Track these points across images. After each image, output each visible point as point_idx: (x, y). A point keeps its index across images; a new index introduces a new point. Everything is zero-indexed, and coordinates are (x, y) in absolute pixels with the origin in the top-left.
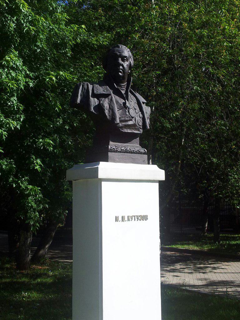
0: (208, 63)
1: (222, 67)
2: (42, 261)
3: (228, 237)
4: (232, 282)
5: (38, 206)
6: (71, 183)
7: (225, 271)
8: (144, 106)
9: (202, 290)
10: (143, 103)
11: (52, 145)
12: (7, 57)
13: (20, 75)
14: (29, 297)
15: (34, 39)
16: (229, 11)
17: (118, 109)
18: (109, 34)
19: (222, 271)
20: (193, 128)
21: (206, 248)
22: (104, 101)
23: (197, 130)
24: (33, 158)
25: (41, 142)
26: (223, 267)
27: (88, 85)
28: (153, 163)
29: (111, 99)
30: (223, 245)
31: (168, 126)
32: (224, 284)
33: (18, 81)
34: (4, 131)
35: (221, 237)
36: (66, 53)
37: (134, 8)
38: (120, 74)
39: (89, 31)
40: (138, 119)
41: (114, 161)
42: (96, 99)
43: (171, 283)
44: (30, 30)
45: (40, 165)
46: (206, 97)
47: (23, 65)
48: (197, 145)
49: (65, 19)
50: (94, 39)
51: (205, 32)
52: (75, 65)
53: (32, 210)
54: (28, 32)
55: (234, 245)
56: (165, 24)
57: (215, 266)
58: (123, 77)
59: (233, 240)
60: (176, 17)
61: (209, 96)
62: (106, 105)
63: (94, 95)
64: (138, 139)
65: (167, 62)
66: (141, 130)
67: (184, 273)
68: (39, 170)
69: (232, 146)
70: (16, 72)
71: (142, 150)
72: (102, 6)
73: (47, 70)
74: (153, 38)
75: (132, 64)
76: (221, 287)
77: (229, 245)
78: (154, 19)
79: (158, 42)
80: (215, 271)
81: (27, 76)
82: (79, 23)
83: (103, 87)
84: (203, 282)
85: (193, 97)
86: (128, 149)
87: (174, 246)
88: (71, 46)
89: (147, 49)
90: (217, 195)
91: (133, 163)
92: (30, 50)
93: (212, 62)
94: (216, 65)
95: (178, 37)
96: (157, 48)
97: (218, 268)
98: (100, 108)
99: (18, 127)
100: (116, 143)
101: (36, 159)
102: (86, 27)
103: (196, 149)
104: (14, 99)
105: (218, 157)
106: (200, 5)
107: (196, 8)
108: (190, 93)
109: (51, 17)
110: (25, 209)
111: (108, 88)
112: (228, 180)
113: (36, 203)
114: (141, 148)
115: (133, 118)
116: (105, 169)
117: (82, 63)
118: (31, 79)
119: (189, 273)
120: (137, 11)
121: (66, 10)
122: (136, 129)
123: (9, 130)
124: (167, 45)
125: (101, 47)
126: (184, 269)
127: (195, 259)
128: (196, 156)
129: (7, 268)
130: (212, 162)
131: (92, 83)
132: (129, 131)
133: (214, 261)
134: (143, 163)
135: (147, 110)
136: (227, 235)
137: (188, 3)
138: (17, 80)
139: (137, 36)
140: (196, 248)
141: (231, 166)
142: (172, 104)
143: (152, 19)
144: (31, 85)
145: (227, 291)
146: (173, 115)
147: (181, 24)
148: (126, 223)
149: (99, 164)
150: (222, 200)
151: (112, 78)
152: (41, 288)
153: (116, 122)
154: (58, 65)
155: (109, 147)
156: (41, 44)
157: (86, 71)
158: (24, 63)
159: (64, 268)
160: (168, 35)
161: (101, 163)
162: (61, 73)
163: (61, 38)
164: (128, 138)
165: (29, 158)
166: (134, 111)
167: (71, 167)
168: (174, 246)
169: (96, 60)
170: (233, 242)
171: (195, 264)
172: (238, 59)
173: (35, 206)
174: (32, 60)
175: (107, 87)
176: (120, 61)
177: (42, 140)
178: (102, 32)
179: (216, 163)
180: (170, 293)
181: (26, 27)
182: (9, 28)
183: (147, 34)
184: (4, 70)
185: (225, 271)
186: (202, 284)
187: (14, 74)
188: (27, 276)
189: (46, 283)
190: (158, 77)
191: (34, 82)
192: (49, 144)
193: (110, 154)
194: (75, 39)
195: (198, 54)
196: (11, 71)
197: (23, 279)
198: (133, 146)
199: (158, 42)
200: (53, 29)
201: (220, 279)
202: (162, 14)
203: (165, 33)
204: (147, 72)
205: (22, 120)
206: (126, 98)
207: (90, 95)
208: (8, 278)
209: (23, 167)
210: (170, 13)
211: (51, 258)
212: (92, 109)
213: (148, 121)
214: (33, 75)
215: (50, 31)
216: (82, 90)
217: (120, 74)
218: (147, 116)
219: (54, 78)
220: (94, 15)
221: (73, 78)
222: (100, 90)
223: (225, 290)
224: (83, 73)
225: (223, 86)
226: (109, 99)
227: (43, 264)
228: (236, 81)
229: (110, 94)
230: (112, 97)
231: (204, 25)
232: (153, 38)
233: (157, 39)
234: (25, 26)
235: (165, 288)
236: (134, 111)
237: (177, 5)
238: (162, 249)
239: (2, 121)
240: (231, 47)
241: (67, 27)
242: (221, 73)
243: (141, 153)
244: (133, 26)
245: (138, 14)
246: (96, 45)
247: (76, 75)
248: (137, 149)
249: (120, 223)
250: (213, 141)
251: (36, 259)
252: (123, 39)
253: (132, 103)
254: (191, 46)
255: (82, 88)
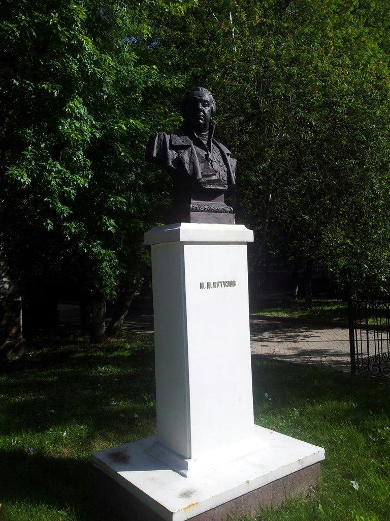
0: (298, 106)
1: (314, 110)
2: (117, 334)
3: (321, 302)
4: (326, 351)
5: (114, 272)
6: (148, 247)
7: (319, 339)
8: (228, 158)
9: (293, 360)
10: (228, 154)
11: (126, 203)
12: (70, 103)
13: (86, 126)
14: (106, 372)
15: (100, 83)
16: (321, 44)
17: (200, 162)
18: (184, 74)
19: (315, 339)
20: (282, 182)
21: (296, 315)
22: (183, 154)
23: (286, 184)
24: (105, 219)
25: (112, 201)
26: (316, 335)
27: (164, 135)
28: (238, 222)
29: (192, 151)
30: (315, 311)
31: (254, 178)
32: (318, 353)
33: (83, 132)
34: (72, 189)
35: (313, 302)
36: (136, 99)
37: (212, 44)
38: (201, 121)
39: (161, 72)
40: (222, 173)
41: (197, 221)
42: (174, 152)
43: (260, 353)
44: (95, 73)
45: (114, 226)
46: (296, 145)
47: (88, 114)
48: (287, 201)
49: (133, 59)
50: (167, 82)
51: (295, 70)
52: (146, 112)
53: (107, 276)
54: (94, 73)
55: (328, 311)
56: (248, 62)
57: (307, 334)
58: (205, 125)
59: (327, 305)
60: (261, 53)
61: (300, 144)
62: (186, 158)
63: (172, 147)
64: (223, 195)
65: (252, 106)
66: (226, 186)
67: (274, 342)
68: (113, 231)
69: (325, 201)
70: (81, 123)
71: (228, 209)
72: (175, 42)
73: (114, 118)
74: (234, 79)
75: (214, 110)
76: (314, 356)
77: (322, 310)
78: (236, 55)
79: (241, 83)
80: (307, 339)
81: (93, 126)
82: (149, 63)
83: (182, 137)
84: (295, 351)
85: (282, 145)
86: (212, 207)
87: (261, 314)
88: (142, 90)
89: (228, 92)
90: (309, 256)
91: (217, 223)
92: (95, 96)
93: (302, 105)
94: (309, 109)
95: (263, 77)
96: (240, 90)
97: (311, 336)
98: (179, 161)
99: (87, 185)
100: (198, 201)
101: (109, 220)
102: (158, 67)
103: (285, 205)
104: (80, 153)
105: (311, 214)
106: (288, 38)
107: (284, 41)
108: (279, 142)
109: (118, 57)
110: (98, 277)
111: (188, 138)
112: (321, 240)
113: (111, 269)
114: (226, 206)
115: (216, 172)
116: (187, 230)
117: (155, 109)
118: (97, 129)
119: (279, 342)
120: (215, 47)
121: (134, 48)
122: (221, 185)
123: (78, 188)
124: (251, 86)
125: (176, 90)
126: (273, 337)
127: (285, 327)
128: (285, 214)
129: (81, 342)
130: (304, 220)
131: (169, 133)
132: (213, 187)
133: (306, 329)
134: (230, 222)
135: (232, 162)
136: (333, 300)
137: (274, 36)
138: (82, 132)
139: (217, 78)
140: (286, 315)
141: (325, 224)
142: (257, 155)
143: (233, 56)
144: (98, 135)
145: (321, 361)
146: (259, 167)
147: (267, 61)
148: (212, 290)
149: (180, 226)
150: (314, 262)
151: (192, 126)
152: (119, 362)
153: (198, 178)
154: (127, 113)
155: (191, 206)
156: (108, 89)
157: (159, 119)
158: (90, 112)
159: (142, 340)
160: (252, 74)
161: (182, 224)
162: (131, 121)
163: (130, 82)
164: (211, 195)
165: (101, 219)
166: (217, 164)
167: (148, 229)
168: (261, 314)
169: (169, 106)
170: (327, 308)
171: (285, 332)
172: (333, 101)
173: (110, 272)
174: (97, 108)
175: (187, 137)
176: (201, 107)
177: (114, 198)
178: (176, 73)
179: (308, 220)
180: (259, 364)
181: (91, 68)
182: (71, 71)
183: (228, 75)
184: (67, 120)
185: (319, 339)
186: (294, 354)
187: (78, 125)
188: (102, 349)
189: (123, 356)
190: (241, 123)
191: (101, 132)
192: (122, 203)
193: (192, 214)
194: (145, 82)
195: (287, 96)
196: (75, 121)
197: (99, 353)
198: (217, 204)
199: (241, 83)
200: (120, 71)
201: (313, 348)
202: (245, 49)
203: (248, 72)
204: (228, 119)
205: (90, 177)
206: (208, 149)
207: (168, 146)
208: (81, 352)
209: (95, 231)
210: (254, 48)
211: (127, 330)
212: (171, 163)
213: (233, 176)
214: (99, 126)
215: (117, 73)
216: (159, 141)
217: (201, 121)
218: (232, 169)
219: (124, 127)
220: (166, 53)
221: (145, 127)
222: (179, 140)
223: (319, 359)
224: (156, 121)
225: (315, 132)
226: (189, 151)
227: (119, 336)
228: (330, 126)
229: (190, 146)
230: (192, 149)
231: (294, 61)
232: (234, 79)
233: (240, 80)
234: (89, 67)
235: (256, 359)
236: (217, 164)
237: (262, 38)
238: (251, 318)
239: (68, 177)
240: (324, 87)
241: (137, 69)
242: (313, 118)
243: (226, 212)
244: (211, 65)
245: (217, 51)
246: (170, 88)
247: (148, 123)
248: (222, 207)
249: (205, 290)
250: (304, 195)
251: (111, 332)
252: (197, 81)
253: (215, 155)
254: (278, 87)
255: (159, 139)
